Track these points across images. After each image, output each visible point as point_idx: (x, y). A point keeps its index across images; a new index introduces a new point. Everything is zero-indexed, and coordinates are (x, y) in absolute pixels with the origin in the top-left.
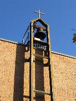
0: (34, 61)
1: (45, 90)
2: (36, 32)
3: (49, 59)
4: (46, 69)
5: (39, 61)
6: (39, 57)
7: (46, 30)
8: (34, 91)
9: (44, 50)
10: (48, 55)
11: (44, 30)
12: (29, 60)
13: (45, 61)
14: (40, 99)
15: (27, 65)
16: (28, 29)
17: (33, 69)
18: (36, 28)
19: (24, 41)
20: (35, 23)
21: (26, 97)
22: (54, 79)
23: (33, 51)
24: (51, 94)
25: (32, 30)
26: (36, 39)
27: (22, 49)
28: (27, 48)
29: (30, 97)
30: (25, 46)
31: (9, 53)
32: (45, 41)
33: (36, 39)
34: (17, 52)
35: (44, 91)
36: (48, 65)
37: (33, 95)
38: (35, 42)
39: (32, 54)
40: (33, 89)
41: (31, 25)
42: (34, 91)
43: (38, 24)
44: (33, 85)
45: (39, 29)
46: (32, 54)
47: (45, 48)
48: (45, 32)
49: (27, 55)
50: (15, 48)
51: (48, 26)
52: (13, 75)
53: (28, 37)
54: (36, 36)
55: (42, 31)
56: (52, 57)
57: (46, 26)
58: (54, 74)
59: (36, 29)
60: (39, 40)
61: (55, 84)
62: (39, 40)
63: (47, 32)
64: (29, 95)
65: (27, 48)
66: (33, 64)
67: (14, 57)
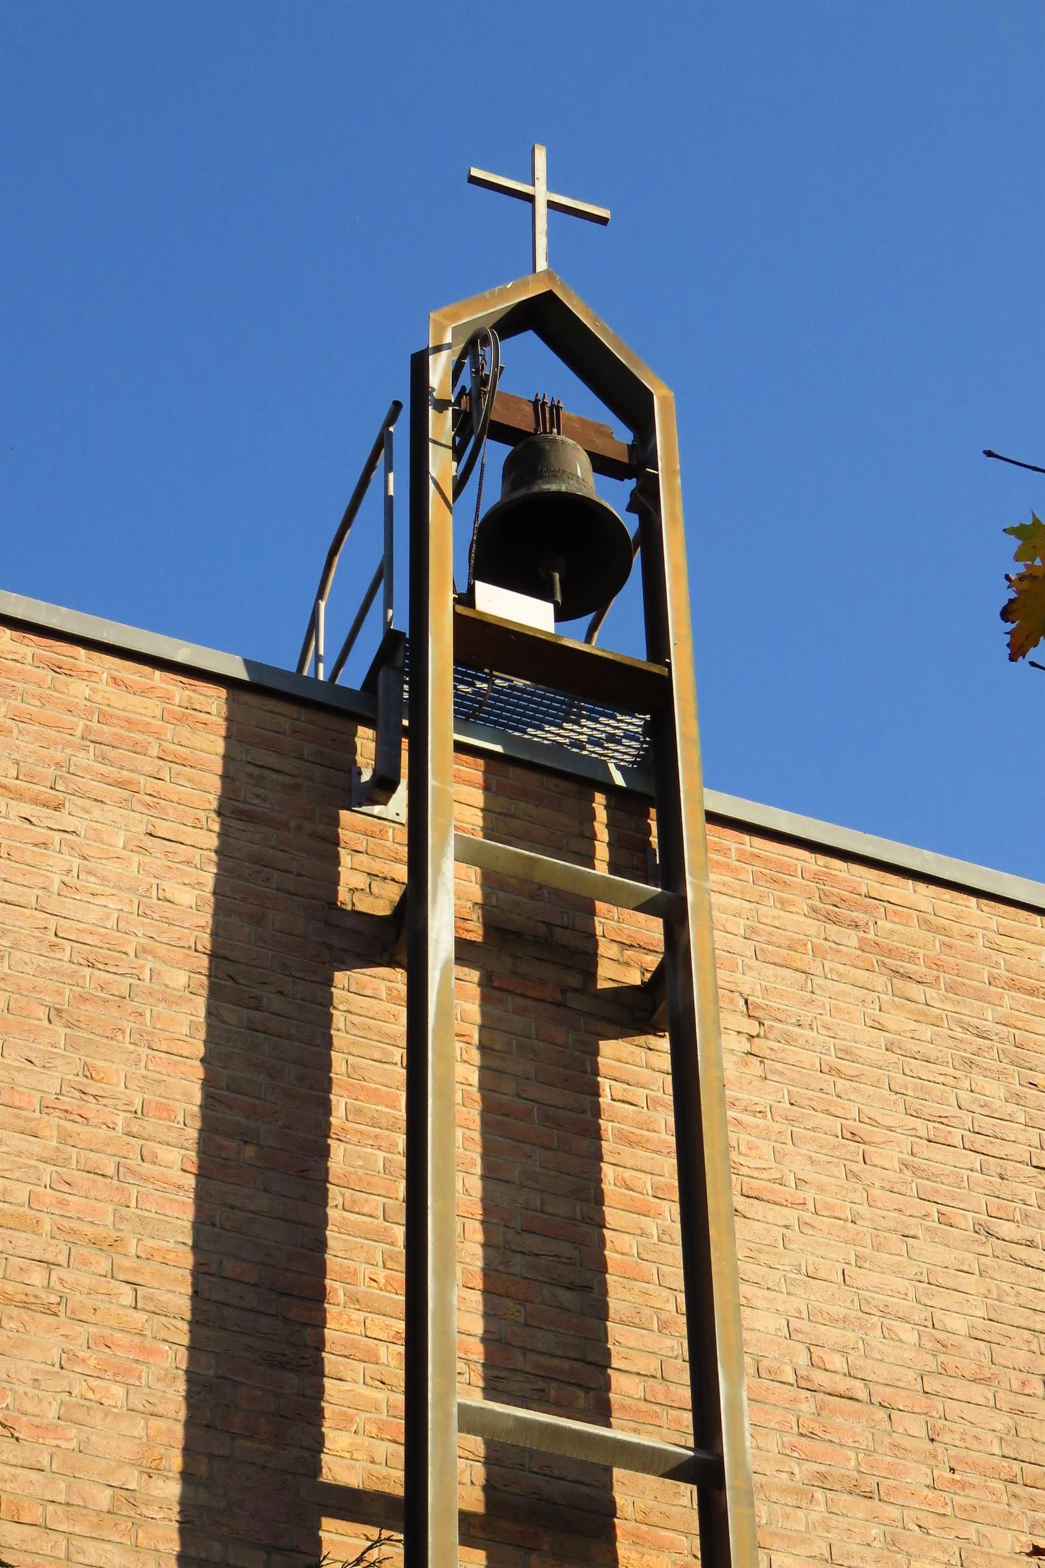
0: (465, 952)
1: (623, 1389)
2: (491, 490)
3: (674, 915)
4: (632, 1071)
5: (531, 947)
6: (539, 891)
7: (637, 466)
8: (469, 1421)
9: (600, 778)
10: (659, 872)
11: (602, 465)
12: (397, 938)
13: (625, 945)
14: (552, 1536)
15: (366, 1000)
16: (383, 442)
17: (457, 1071)
18: (501, 432)
19: (337, 657)
20: (474, 344)
21: (354, 1505)
22: (736, 1243)
23: (459, 798)
24: (704, 1471)
25: (441, 465)
26: (498, 603)
27: (300, 751)
28: (365, 741)
29: (407, 1513)
30: (337, 710)
31: (120, 825)
32: (617, 636)
33: (498, 603)
34: (232, 809)
35: (602, 1413)
36: (663, 1005)
37: (459, 1479)
38: (482, 643)
39: (434, 840)
40: (458, 1383)
41: (419, 365)
42: (467, 854)
43: (530, 372)
44: (461, 1312)
45: (529, 453)
46: (434, 840)
47: (608, 741)
48: (614, 497)
49: (366, 862)
50: (210, 745)
51: (661, 395)
52: (176, 1159)
53: (384, 573)
54: (503, 551)
55: (579, 476)
56: (724, 884)
57: (631, 404)
58: (741, 1144)
59: (495, 454)
60: (531, 613)
61: (755, 1320)
62: (531, 613)
63: (646, 501)
64: (394, 1482)
65: (365, 741)
66: (457, 998)
67: (189, 892)
